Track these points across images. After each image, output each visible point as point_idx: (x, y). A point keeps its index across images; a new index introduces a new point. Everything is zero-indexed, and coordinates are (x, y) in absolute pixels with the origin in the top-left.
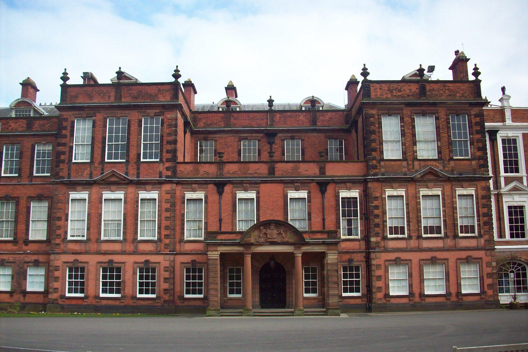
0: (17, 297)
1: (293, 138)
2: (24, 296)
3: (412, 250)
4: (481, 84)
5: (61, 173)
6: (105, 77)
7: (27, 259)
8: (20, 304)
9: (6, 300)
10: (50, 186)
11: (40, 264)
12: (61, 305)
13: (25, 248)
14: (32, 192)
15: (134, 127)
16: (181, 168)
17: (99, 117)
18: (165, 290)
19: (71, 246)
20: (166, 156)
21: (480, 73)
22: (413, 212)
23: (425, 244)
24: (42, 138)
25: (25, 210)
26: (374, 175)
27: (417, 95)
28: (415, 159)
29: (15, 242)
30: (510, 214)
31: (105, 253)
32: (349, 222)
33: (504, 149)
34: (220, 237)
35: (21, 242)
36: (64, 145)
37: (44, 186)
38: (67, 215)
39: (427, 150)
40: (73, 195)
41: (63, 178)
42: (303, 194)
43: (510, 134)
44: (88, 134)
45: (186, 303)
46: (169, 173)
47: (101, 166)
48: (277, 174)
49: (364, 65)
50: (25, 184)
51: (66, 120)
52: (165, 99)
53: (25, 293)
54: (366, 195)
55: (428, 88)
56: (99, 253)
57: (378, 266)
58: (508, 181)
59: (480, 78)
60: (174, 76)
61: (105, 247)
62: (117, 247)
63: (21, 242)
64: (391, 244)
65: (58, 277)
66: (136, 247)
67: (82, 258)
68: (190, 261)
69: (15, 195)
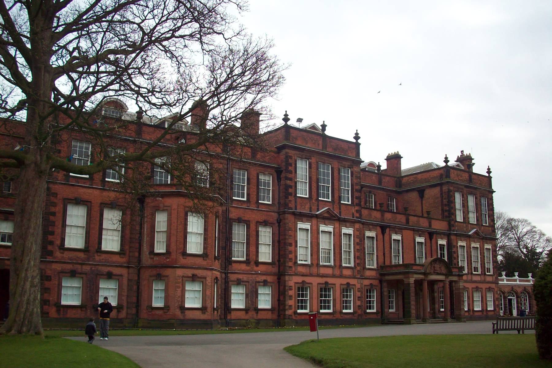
0: (252, 313)
2: (257, 313)
4: (361, 146)
5: (290, 204)
7: (258, 279)
8: (254, 321)
9: (243, 317)
10: (273, 214)
11: (113, 277)
12: (295, 320)
13: (256, 268)
14: (260, 217)
18: (359, 306)
19: (300, 269)
20: (356, 201)
21: (359, 138)
25: (254, 233)
28: (469, 223)
29: (247, 262)
31: (323, 276)
34: (415, 268)
35: (252, 263)
36: (291, 179)
37: (268, 213)
38: (296, 242)
40: (300, 225)
41: (291, 208)
45: (368, 316)
46: (358, 215)
47: (316, 203)
48: (410, 223)
49: (286, 111)
50: (254, 209)
51: (291, 157)
53: (257, 310)
56: (318, 275)
59: (359, 141)
60: (444, 161)
61: (322, 271)
62: (329, 271)
63: (252, 263)
65: (292, 296)
66: (341, 272)
67: (308, 279)
68: (324, 282)
69: (246, 219)
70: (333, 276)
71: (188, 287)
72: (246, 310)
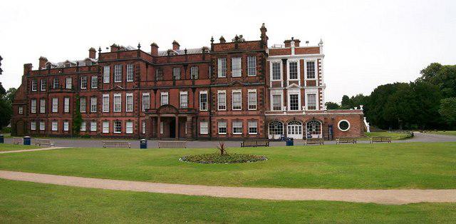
1: (194, 66)
3: (244, 116)
6: (229, 40)
15: (124, 68)
16: (142, 84)
17: (112, 65)
22: (229, 99)
23: (234, 113)
24: (94, 74)
26: (214, 84)
27: (238, 47)
29: (86, 113)
30: (291, 98)
31: (115, 117)
32: (204, 104)
33: (290, 67)
39: (237, 73)
40: (104, 95)
42: (186, 93)
43: (293, 60)
44: (109, 72)
52: (135, 56)
53: (90, 132)
54: (210, 93)
55: (239, 45)
56: (113, 117)
57: (214, 122)
58: (290, 83)
61: (115, 115)
62: (120, 114)
64: (220, 113)
70: (122, 116)
71: (53, 123)
72: (86, 132)
